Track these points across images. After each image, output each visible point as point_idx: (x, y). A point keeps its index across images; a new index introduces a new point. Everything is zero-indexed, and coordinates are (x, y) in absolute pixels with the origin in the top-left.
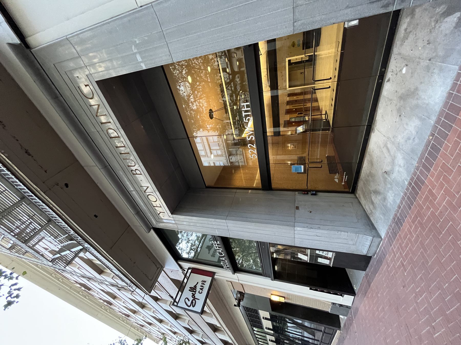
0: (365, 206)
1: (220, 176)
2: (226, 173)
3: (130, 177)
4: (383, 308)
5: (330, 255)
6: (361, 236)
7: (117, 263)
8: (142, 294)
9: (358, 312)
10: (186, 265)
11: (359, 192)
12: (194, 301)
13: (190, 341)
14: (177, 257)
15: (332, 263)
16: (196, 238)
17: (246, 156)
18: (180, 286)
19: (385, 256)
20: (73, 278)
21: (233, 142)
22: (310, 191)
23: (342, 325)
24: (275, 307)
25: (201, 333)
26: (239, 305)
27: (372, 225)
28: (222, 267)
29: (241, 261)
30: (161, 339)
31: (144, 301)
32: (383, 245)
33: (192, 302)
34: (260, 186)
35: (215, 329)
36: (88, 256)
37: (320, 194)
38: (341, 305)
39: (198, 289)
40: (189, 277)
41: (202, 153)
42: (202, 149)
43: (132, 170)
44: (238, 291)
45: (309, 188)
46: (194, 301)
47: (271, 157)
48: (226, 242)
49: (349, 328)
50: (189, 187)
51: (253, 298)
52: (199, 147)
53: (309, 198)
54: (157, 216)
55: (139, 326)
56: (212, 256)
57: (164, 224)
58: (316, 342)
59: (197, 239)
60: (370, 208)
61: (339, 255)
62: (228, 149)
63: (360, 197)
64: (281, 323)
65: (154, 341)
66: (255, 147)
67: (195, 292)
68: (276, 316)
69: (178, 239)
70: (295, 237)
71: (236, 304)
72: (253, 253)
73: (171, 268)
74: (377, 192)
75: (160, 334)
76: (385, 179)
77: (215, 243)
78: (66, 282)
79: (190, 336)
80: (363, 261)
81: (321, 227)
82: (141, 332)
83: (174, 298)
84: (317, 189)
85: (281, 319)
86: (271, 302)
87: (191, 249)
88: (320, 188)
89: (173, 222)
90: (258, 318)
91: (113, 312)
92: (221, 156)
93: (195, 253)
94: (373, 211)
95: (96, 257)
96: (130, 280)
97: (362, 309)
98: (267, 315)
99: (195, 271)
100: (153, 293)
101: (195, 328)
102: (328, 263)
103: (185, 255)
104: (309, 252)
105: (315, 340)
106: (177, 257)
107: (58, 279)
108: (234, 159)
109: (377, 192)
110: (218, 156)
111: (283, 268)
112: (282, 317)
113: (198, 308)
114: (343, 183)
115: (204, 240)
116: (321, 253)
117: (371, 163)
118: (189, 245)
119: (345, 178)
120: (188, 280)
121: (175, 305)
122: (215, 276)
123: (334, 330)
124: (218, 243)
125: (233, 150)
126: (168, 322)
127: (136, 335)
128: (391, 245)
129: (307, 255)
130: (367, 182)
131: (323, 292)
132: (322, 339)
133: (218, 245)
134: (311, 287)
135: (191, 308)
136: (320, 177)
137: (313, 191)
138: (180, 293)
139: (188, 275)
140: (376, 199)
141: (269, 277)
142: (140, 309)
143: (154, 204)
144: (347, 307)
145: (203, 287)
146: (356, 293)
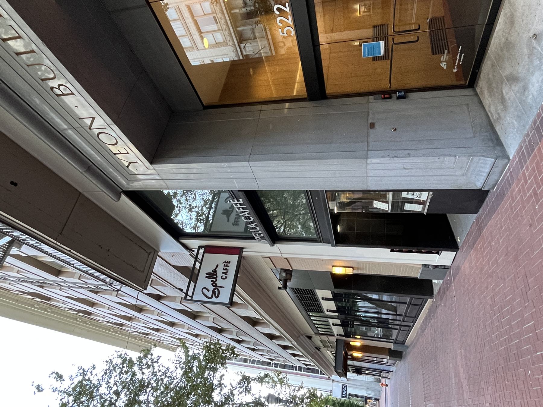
0: (490, 107)
1: (226, 84)
2: (239, 73)
3: (54, 103)
4: (496, 260)
5: (424, 196)
6: (476, 159)
7: (79, 254)
8: (134, 293)
9: (460, 272)
10: (194, 244)
11: (482, 84)
12: (216, 290)
13: (221, 342)
14: (177, 233)
15: (426, 209)
16: (202, 203)
17: (273, 39)
18: (191, 274)
19: (510, 185)
20: (16, 288)
21: (244, 10)
22: (395, 92)
23: (436, 291)
24: (339, 281)
25: (235, 331)
26: (285, 287)
27: (498, 139)
28: (253, 238)
29: (282, 229)
30: (179, 346)
31: (139, 303)
32: (509, 168)
33: (214, 292)
34: (304, 94)
35: (253, 322)
36: (26, 251)
37: (413, 96)
38: (436, 267)
40: (202, 260)
41: (185, 42)
42: (177, 17)
43: (52, 88)
44: (281, 269)
45: (394, 86)
46: (216, 290)
47: (323, 38)
48: (254, 199)
49: (445, 293)
50: (172, 111)
51: (306, 274)
52: (178, 29)
53: (394, 104)
54: (124, 170)
55: (141, 335)
56: (234, 225)
57: (140, 183)
59: (205, 205)
60: (497, 111)
61: (438, 195)
62: (236, 27)
63: (482, 92)
64: (348, 302)
65: (169, 349)
66: (287, 10)
67: (216, 278)
68: (341, 295)
69: (173, 207)
70: (368, 175)
71: (281, 286)
72: (300, 214)
74: (513, 79)
75: (175, 340)
76: (532, 49)
77: (236, 202)
78: (56, 311)
79: (219, 336)
80: (474, 200)
81: (412, 152)
82: (146, 342)
83: (185, 291)
84: (408, 87)
85: (348, 297)
86: (333, 276)
87: (198, 220)
88: (413, 82)
89: (157, 177)
90: (316, 300)
91: (97, 324)
92: (224, 44)
93: (205, 225)
94: (502, 115)
95: (41, 250)
96: (109, 276)
97: (466, 267)
98: (328, 294)
99: (209, 249)
100: (150, 290)
101: (224, 325)
102: (420, 210)
103: (188, 230)
104: (390, 196)
105: (397, 315)
106: (177, 233)
107: (46, 310)
108: (251, 49)
109: (513, 79)
110: (217, 45)
111: (349, 228)
112: (349, 294)
113: (224, 297)
114: (455, 70)
115: (217, 203)
116: (410, 196)
117: (512, 22)
118: (194, 214)
119: (460, 58)
120: (201, 263)
121: (188, 300)
122: (244, 253)
124: (241, 201)
125: (247, 29)
126: (184, 324)
127: (140, 346)
128: (522, 167)
129: (387, 202)
130: (499, 58)
131: (411, 252)
133: (240, 204)
134: (393, 248)
135: (214, 299)
136: (414, 61)
137: (400, 91)
138: (192, 284)
139: (200, 257)
140: (510, 92)
141: (329, 243)
142: (137, 314)
143: (114, 149)
144: (445, 267)
145: (226, 269)
146: (460, 247)
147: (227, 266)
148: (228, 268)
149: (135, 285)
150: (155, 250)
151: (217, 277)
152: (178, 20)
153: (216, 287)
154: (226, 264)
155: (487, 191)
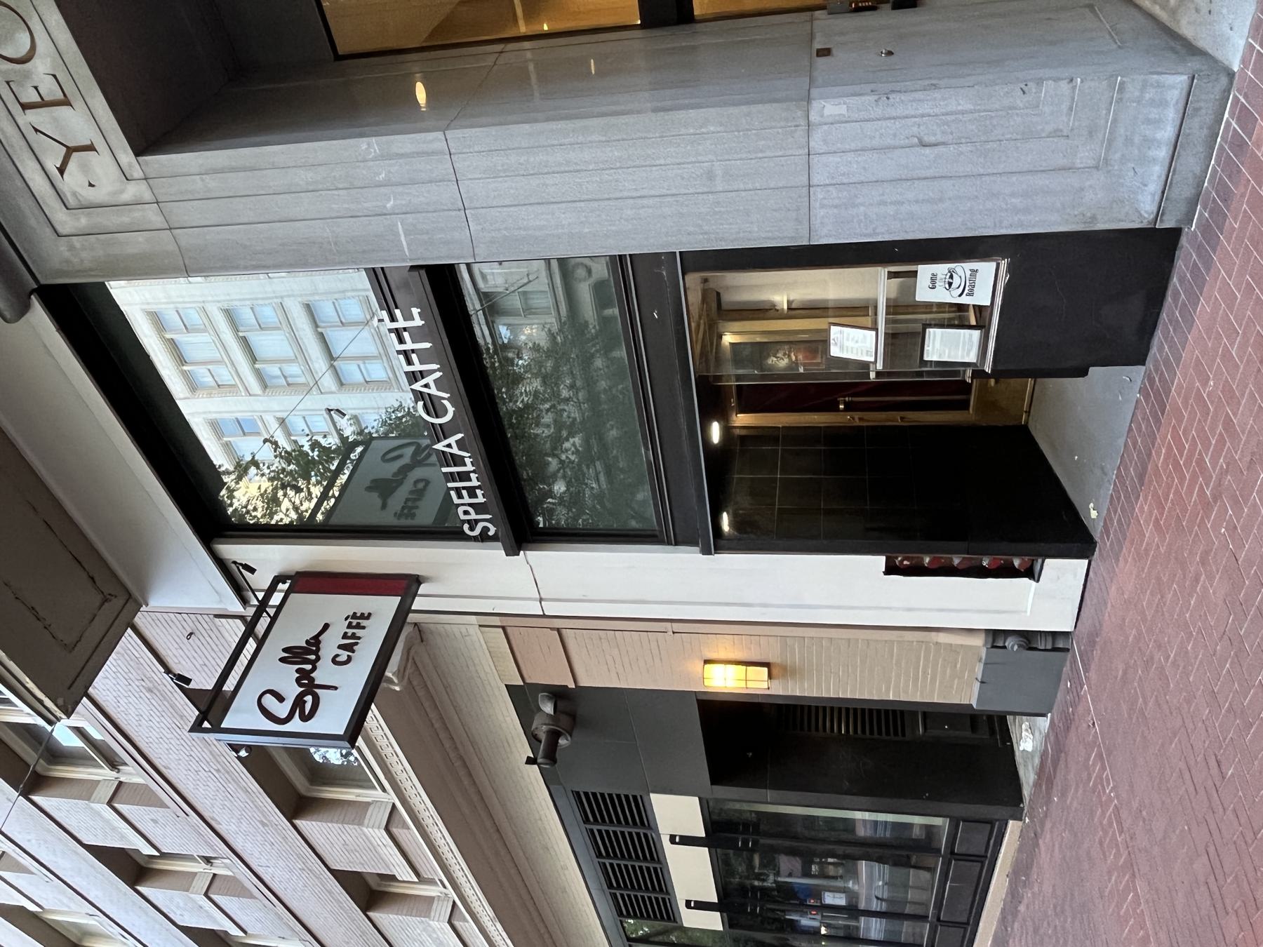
12: (309, 699)
14: (212, 521)
39: (330, 646)
46: (309, 699)
58: (906, 930)
70: (814, 181)
73: (187, 594)
123: (991, 823)
132: (939, 906)
141: (696, 544)
146: (1097, 537)
147: (358, 626)
148: (359, 632)
149: (30, 685)
150: (130, 596)
151: (318, 658)
152: (374, 357)
153: (307, 682)
154: (355, 622)
155: (1175, 234)
